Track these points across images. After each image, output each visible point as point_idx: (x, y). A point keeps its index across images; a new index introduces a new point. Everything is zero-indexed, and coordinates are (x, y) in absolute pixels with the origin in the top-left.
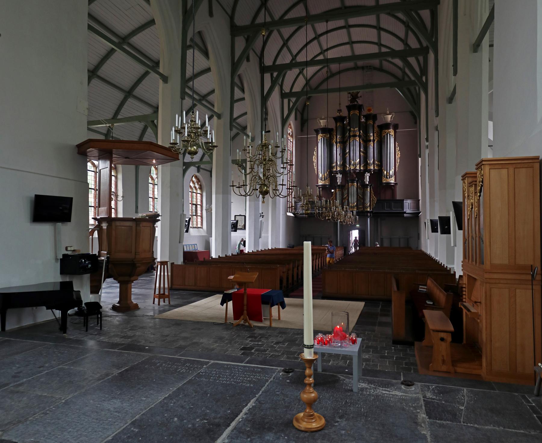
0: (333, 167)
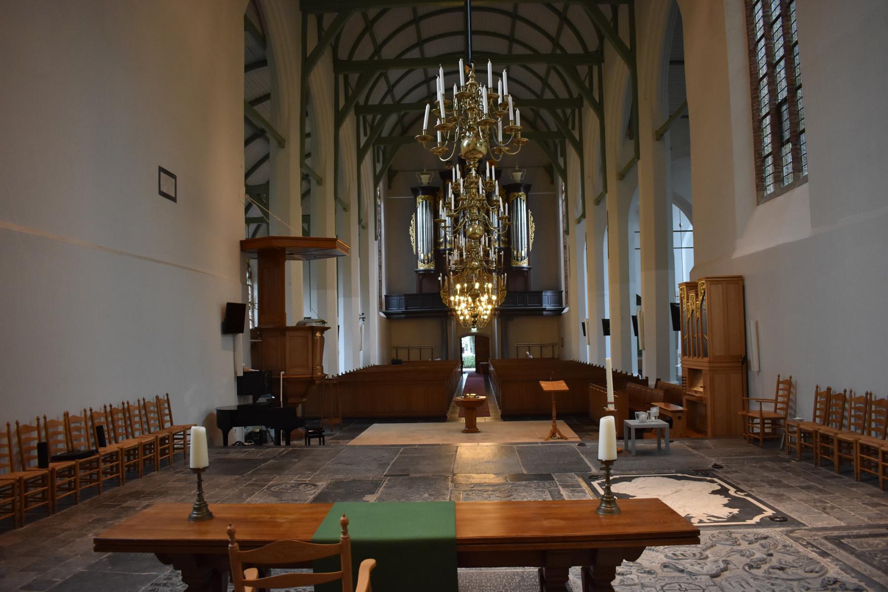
0: (441, 244)
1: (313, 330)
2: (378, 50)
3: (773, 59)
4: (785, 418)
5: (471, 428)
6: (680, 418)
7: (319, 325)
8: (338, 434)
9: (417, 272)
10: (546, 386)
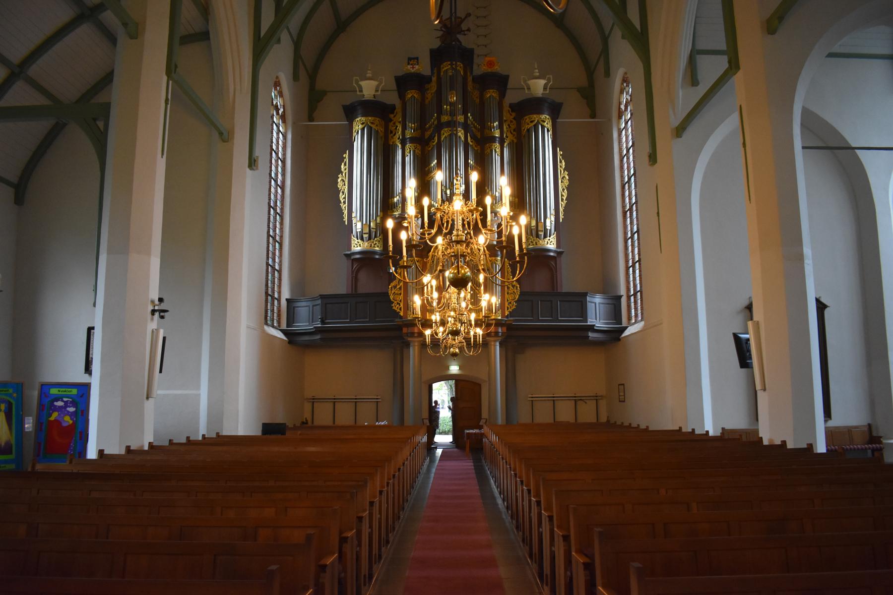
9: (348, 256)
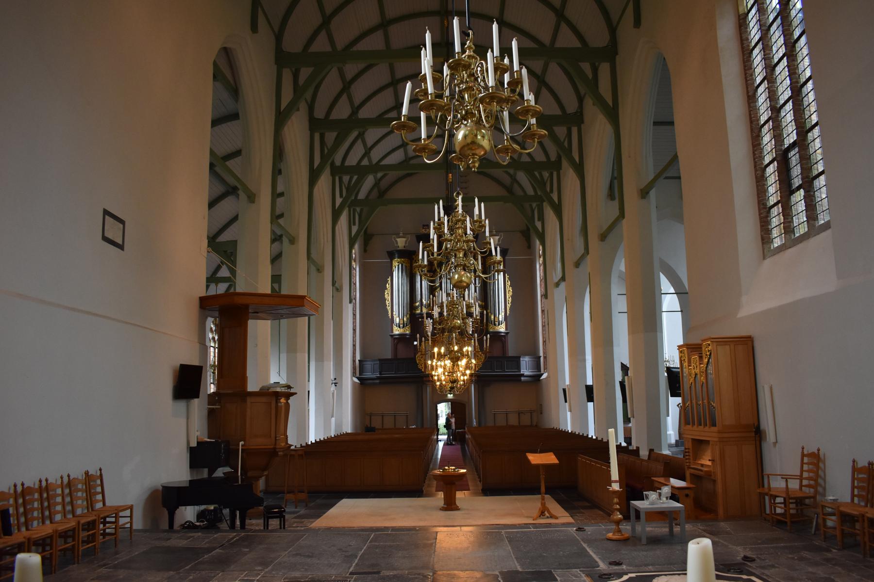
0: (416, 308)
1: (277, 395)
2: (355, 110)
3: (777, 103)
4: (814, 497)
5: (450, 505)
6: (687, 496)
7: (283, 390)
8: (303, 512)
9: (392, 336)
10: (535, 458)
